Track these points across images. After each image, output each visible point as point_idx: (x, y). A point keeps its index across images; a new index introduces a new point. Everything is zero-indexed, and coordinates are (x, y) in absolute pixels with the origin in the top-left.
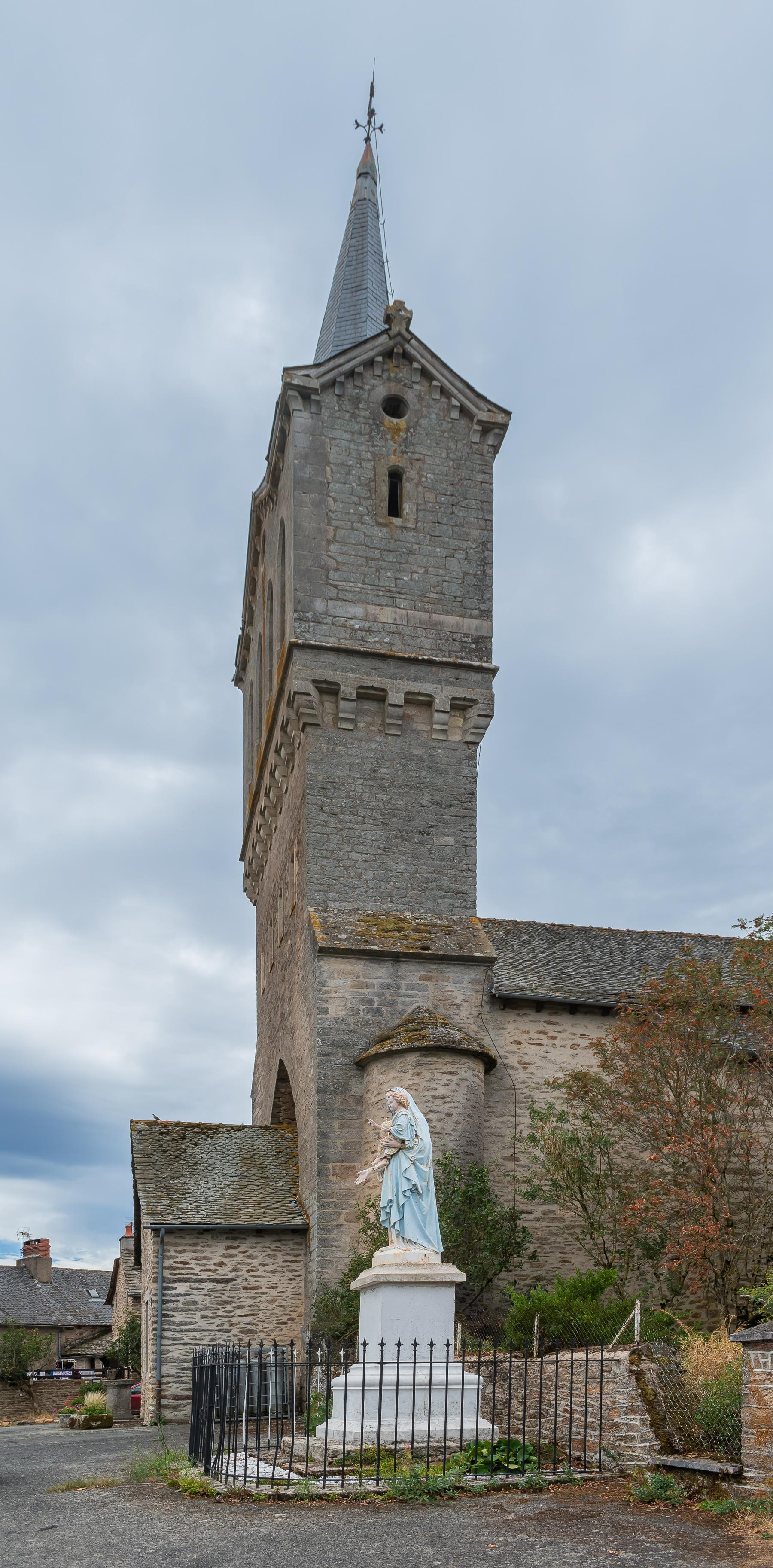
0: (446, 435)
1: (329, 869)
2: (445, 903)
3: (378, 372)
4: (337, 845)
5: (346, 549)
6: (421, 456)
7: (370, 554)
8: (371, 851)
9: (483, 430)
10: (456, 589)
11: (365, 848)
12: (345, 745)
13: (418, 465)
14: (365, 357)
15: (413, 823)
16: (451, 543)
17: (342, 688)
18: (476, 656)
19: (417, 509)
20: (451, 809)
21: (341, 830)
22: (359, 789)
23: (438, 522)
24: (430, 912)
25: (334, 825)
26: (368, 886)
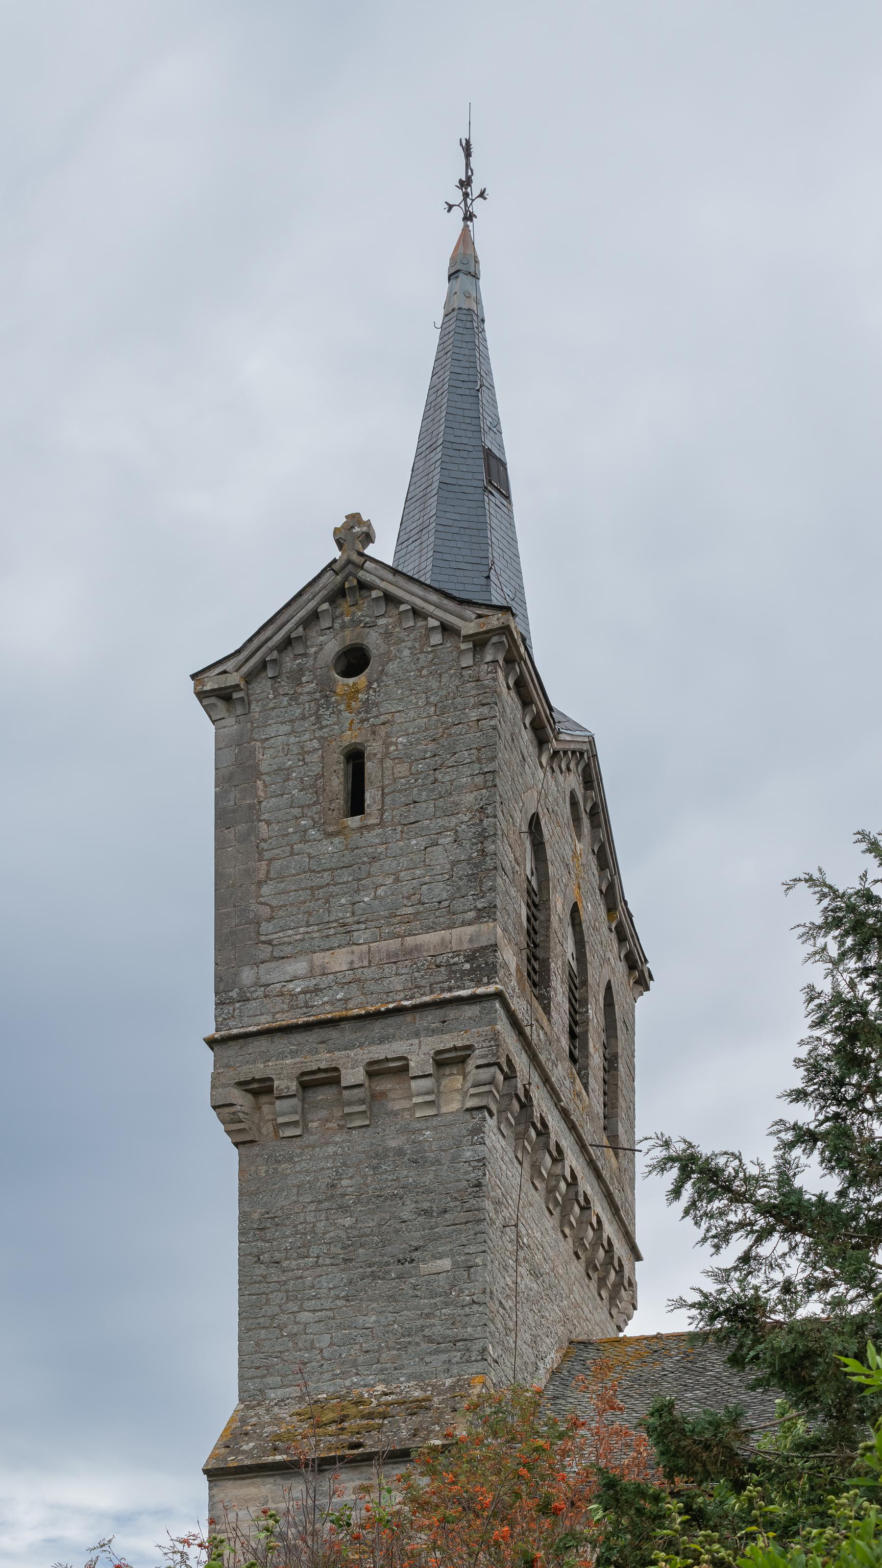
0: (424, 672)
1: (267, 1343)
2: (437, 1361)
3: (325, 623)
4: (280, 1306)
5: (283, 885)
6: (389, 717)
7: (317, 881)
8: (327, 1304)
9: (475, 646)
10: (441, 891)
11: (318, 1302)
12: (290, 1160)
13: (382, 731)
14: (302, 613)
15: (389, 1249)
16: (432, 826)
17: (276, 1083)
18: (472, 980)
19: (383, 794)
20: (447, 1216)
21: (285, 1283)
22: (310, 1218)
23: (415, 802)
24: (415, 1378)
25: (276, 1279)
26: (323, 1358)
